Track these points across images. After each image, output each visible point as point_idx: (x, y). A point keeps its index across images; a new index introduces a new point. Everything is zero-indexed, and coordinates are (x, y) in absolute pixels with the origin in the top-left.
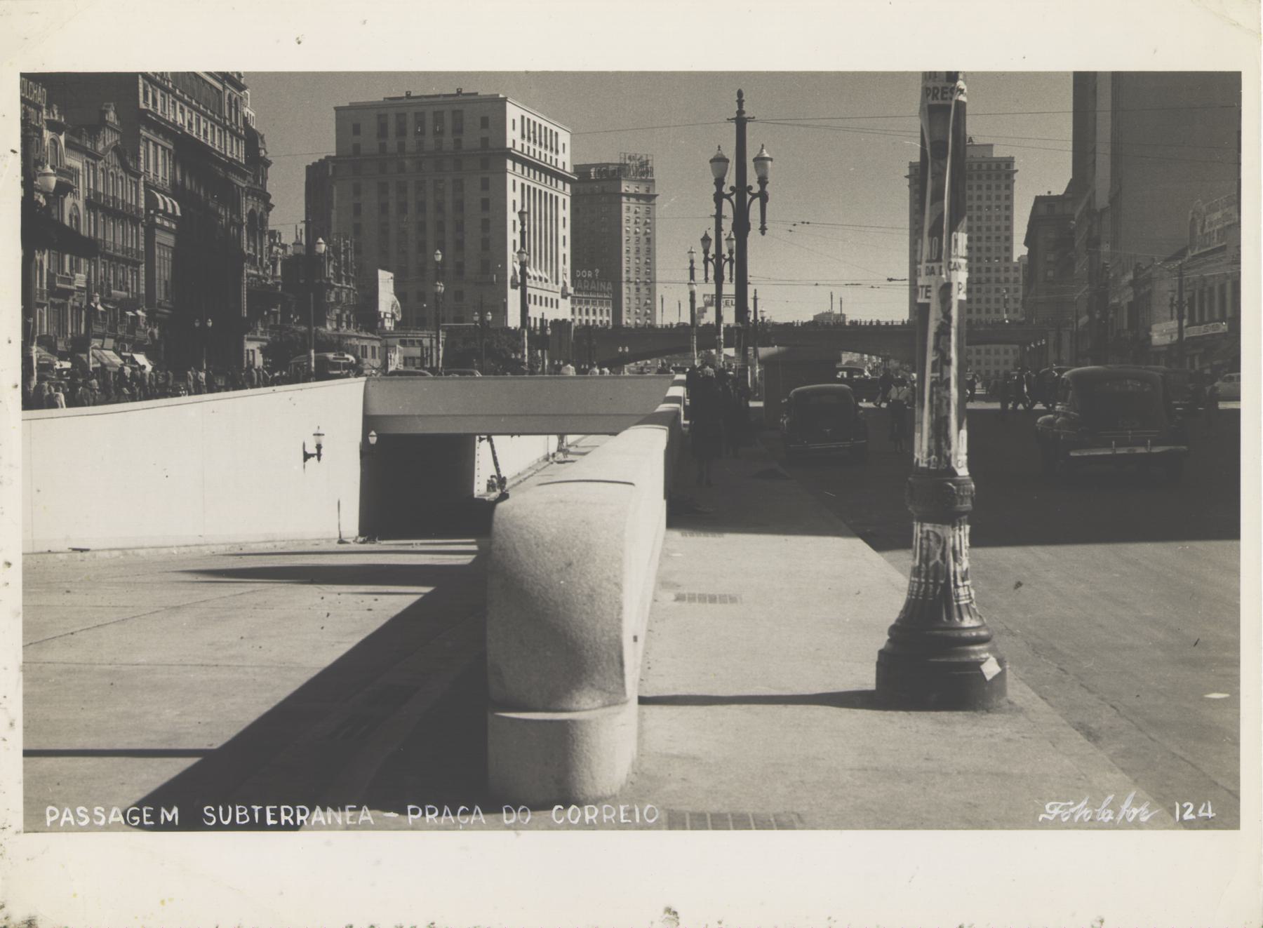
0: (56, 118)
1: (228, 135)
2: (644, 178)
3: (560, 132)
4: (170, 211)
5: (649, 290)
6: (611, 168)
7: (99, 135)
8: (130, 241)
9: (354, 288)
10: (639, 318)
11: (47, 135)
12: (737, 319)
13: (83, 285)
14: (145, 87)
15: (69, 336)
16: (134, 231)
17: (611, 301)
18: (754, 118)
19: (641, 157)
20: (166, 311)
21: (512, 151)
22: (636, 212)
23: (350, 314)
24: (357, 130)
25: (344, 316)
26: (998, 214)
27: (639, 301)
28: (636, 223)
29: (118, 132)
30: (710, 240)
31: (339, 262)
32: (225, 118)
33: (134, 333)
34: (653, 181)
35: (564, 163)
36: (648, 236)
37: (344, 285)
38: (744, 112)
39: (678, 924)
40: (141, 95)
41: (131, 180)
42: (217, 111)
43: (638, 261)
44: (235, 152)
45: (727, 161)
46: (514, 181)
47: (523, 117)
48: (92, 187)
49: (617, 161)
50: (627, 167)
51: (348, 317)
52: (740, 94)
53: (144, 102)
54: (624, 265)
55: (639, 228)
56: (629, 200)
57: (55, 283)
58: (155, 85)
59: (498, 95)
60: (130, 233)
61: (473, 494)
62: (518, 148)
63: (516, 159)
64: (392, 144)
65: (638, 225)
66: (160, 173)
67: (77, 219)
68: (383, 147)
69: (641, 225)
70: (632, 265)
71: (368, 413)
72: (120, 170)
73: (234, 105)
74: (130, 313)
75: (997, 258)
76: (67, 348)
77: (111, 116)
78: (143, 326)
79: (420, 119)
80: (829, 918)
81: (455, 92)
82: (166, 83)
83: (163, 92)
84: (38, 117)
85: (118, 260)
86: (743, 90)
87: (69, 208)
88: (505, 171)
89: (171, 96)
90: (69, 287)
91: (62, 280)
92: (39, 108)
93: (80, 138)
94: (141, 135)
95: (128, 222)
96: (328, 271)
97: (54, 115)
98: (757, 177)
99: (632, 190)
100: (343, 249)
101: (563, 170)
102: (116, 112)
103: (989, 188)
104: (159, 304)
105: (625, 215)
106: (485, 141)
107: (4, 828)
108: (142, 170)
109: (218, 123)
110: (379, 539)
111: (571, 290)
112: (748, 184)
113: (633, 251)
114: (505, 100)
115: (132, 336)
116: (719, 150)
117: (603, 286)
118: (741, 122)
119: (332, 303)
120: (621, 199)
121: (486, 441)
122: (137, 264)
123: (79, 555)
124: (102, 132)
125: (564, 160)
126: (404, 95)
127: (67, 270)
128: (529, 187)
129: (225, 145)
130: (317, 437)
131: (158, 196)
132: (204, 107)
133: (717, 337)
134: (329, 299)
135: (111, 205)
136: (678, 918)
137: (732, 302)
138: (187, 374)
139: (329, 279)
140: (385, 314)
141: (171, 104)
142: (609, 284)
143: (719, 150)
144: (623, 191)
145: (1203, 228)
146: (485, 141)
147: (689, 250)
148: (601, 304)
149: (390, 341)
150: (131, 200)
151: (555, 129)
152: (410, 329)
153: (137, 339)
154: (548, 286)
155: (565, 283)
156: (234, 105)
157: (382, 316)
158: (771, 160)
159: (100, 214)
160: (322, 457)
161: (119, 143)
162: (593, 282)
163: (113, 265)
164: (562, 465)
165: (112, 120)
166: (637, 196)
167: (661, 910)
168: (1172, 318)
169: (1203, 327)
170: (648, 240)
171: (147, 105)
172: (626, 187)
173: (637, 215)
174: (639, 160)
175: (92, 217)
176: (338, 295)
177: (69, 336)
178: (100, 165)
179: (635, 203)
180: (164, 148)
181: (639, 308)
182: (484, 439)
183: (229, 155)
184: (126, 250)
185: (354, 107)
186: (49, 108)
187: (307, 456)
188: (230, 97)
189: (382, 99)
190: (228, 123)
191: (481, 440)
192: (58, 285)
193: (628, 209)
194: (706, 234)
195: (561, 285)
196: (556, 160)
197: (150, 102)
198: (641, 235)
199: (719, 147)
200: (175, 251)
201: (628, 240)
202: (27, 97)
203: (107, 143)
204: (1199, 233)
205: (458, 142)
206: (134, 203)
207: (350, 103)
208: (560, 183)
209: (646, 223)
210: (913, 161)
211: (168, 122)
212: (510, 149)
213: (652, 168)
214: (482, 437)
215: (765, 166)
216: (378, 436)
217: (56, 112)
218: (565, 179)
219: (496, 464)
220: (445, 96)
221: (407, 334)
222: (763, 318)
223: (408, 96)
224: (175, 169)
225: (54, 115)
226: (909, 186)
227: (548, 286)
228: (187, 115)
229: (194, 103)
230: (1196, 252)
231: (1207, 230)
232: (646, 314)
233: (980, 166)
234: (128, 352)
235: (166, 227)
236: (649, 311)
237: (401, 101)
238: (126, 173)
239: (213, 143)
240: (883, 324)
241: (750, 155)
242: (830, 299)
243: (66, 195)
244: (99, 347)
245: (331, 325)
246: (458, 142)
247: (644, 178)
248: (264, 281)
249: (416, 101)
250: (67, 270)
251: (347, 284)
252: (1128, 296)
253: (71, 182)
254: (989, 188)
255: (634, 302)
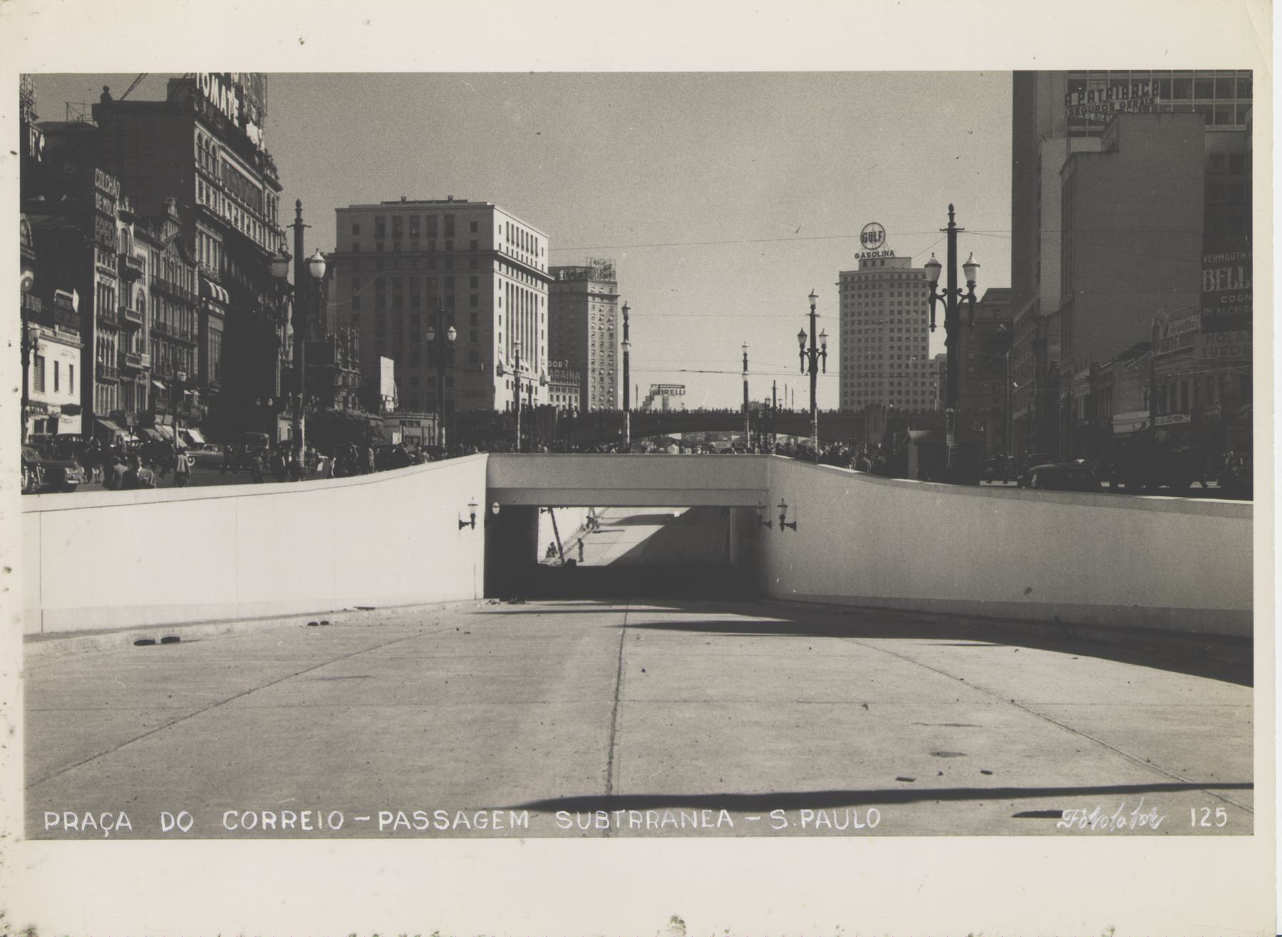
0: (127, 210)
1: (267, 231)
2: (607, 280)
3: (539, 237)
4: (221, 298)
5: (612, 379)
6: (578, 271)
7: (162, 226)
8: (186, 326)
9: (359, 373)
10: (603, 405)
11: (120, 225)
12: (77, 413)
13: (148, 365)
14: (200, 184)
15: (135, 412)
16: (190, 316)
17: (579, 389)
18: (963, 229)
19: (605, 262)
20: (217, 391)
21: (499, 253)
22: (600, 310)
23: (356, 396)
24: (356, 229)
25: (350, 398)
26: (915, 318)
27: (603, 389)
28: (600, 320)
29: (178, 225)
30: (806, 336)
31: (346, 348)
32: (264, 216)
33: (189, 411)
34: (615, 283)
35: (543, 265)
36: (611, 332)
37: (350, 369)
38: (955, 224)
39: (685, 933)
40: (197, 191)
41: (187, 270)
42: (257, 209)
43: (602, 354)
44: (272, 246)
45: (940, 266)
46: (500, 280)
47: (508, 223)
48: (155, 274)
49: (584, 265)
50: (593, 270)
51: (353, 399)
52: (951, 208)
53: (199, 198)
54: (590, 357)
55: (603, 324)
56: (594, 299)
57: (125, 363)
58: (268, 183)
59: (486, 203)
60: (186, 319)
61: (537, 561)
62: (504, 250)
63: (502, 260)
64: (389, 243)
65: (602, 322)
66: (212, 265)
67: (143, 303)
68: (380, 246)
69: (605, 322)
70: (597, 357)
71: (491, 486)
72: (179, 259)
73: (271, 204)
74: (186, 392)
75: (915, 356)
76: (134, 423)
77: (173, 210)
78: (196, 404)
79: (415, 222)
80: (838, 927)
81: (447, 199)
82: (217, 182)
83: (215, 190)
84: (112, 209)
85: (177, 342)
86: (954, 204)
87: (136, 293)
88: (492, 271)
89: (221, 193)
90: (136, 366)
91: (132, 360)
92: (112, 199)
93: (147, 229)
94: (197, 228)
95: (185, 308)
96: (337, 356)
97: (125, 207)
98: (966, 281)
99: (596, 291)
100: (349, 337)
101: (542, 271)
102: (176, 206)
103: (908, 295)
104: (211, 385)
105: (590, 312)
106: (474, 244)
107: (4, 836)
108: (197, 260)
109: (258, 220)
110: (527, 600)
111: (548, 379)
112: (958, 287)
113: (597, 345)
114: (492, 207)
115: (187, 413)
116: (933, 256)
117: (571, 374)
118: (952, 232)
119: (340, 387)
120: (587, 298)
121: (546, 512)
122: (192, 347)
123: (365, 613)
124: (164, 224)
125: (542, 263)
126: (400, 200)
127: (134, 350)
128: (512, 286)
129: (264, 239)
130: (470, 507)
131: (211, 284)
132: (248, 204)
133: (812, 421)
134: (337, 383)
135: (171, 291)
136: (684, 927)
137: (676, 391)
138: (368, 450)
139: (337, 364)
140: (386, 397)
141: (221, 201)
142: (578, 373)
143: (933, 256)
144: (589, 291)
145: (1165, 334)
146: (474, 244)
147: (743, 344)
148: (570, 391)
149: (390, 422)
150: (187, 288)
151: (535, 235)
152: (409, 411)
153: (192, 416)
154: (528, 374)
155: (543, 372)
156: (271, 204)
157: (384, 399)
158: (979, 266)
159: (162, 300)
160: (476, 526)
161: (179, 235)
162: (563, 371)
163: (172, 348)
164: (598, 535)
165: (173, 213)
166: (602, 296)
167: (669, 919)
168: (1146, 410)
169: (1166, 418)
170: (611, 335)
171: (202, 201)
172: (592, 287)
173: (602, 313)
174: (603, 264)
175: (155, 303)
176: (345, 379)
177: (135, 412)
178: (163, 254)
179: (600, 303)
180: (215, 241)
181: (602, 396)
182: (545, 511)
183: (267, 249)
184: (184, 334)
185: (354, 210)
186: (122, 200)
187: (462, 524)
188: (268, 195)
189: (380, 203)
190: (267, 220)
191: (543, 511)
192: (128, 364)
193: (594, 308)
194: (802, 331)
195: (540, 373)
196: (536, 262)
197: (204, 198)
198: (604, 331)
199: (933, 254)
200: (224, 335)
201: (593, 335)
202: (101, 187)
203: (169, 235)
204: (1161, 337)
205: (449, 244)
206: (190, 291)
207: (350, 206)
208: (539, 283)
209: (609, 320)
210: (843, 271)
211: (218, 216)
212: (497, 251)
213: (614, 271)
214: (544, 508)
215: (973, 272)
216: (501, 507)
217: (127, 204)
218: (544, 279)
219: (557, 533)
220: (437, 202)
221: (406, 415)
222: (781, 406)
223: (404, 201)
224: (223, 256)
225: (125, 207)
226: (839, 292)
227: (528, 374)
228: (234, 212)
229: (239, 200)
230: (1159, 353)
231: (1170, 335)
232: (609, 401)
233: (900, 276)
234: (184, 427)
235: (217, 313)
236: (611, 399)
237: (398, 206)
238: (184, 263)
239: (254, 237)
240: (734, 412)
241: (961, 261)
242: (784, 391)
243: (134, 281)
244: (160, 422)
245: (339, 406)
246: (449, 244)
247: (607, 280)
248: (287, 365)
249: (410, 205)
250: (134, 350)
251: (353, 369)
252: (1082, 391)
253: (140, 269)
254: (908, 295)
255: (598, 389)
